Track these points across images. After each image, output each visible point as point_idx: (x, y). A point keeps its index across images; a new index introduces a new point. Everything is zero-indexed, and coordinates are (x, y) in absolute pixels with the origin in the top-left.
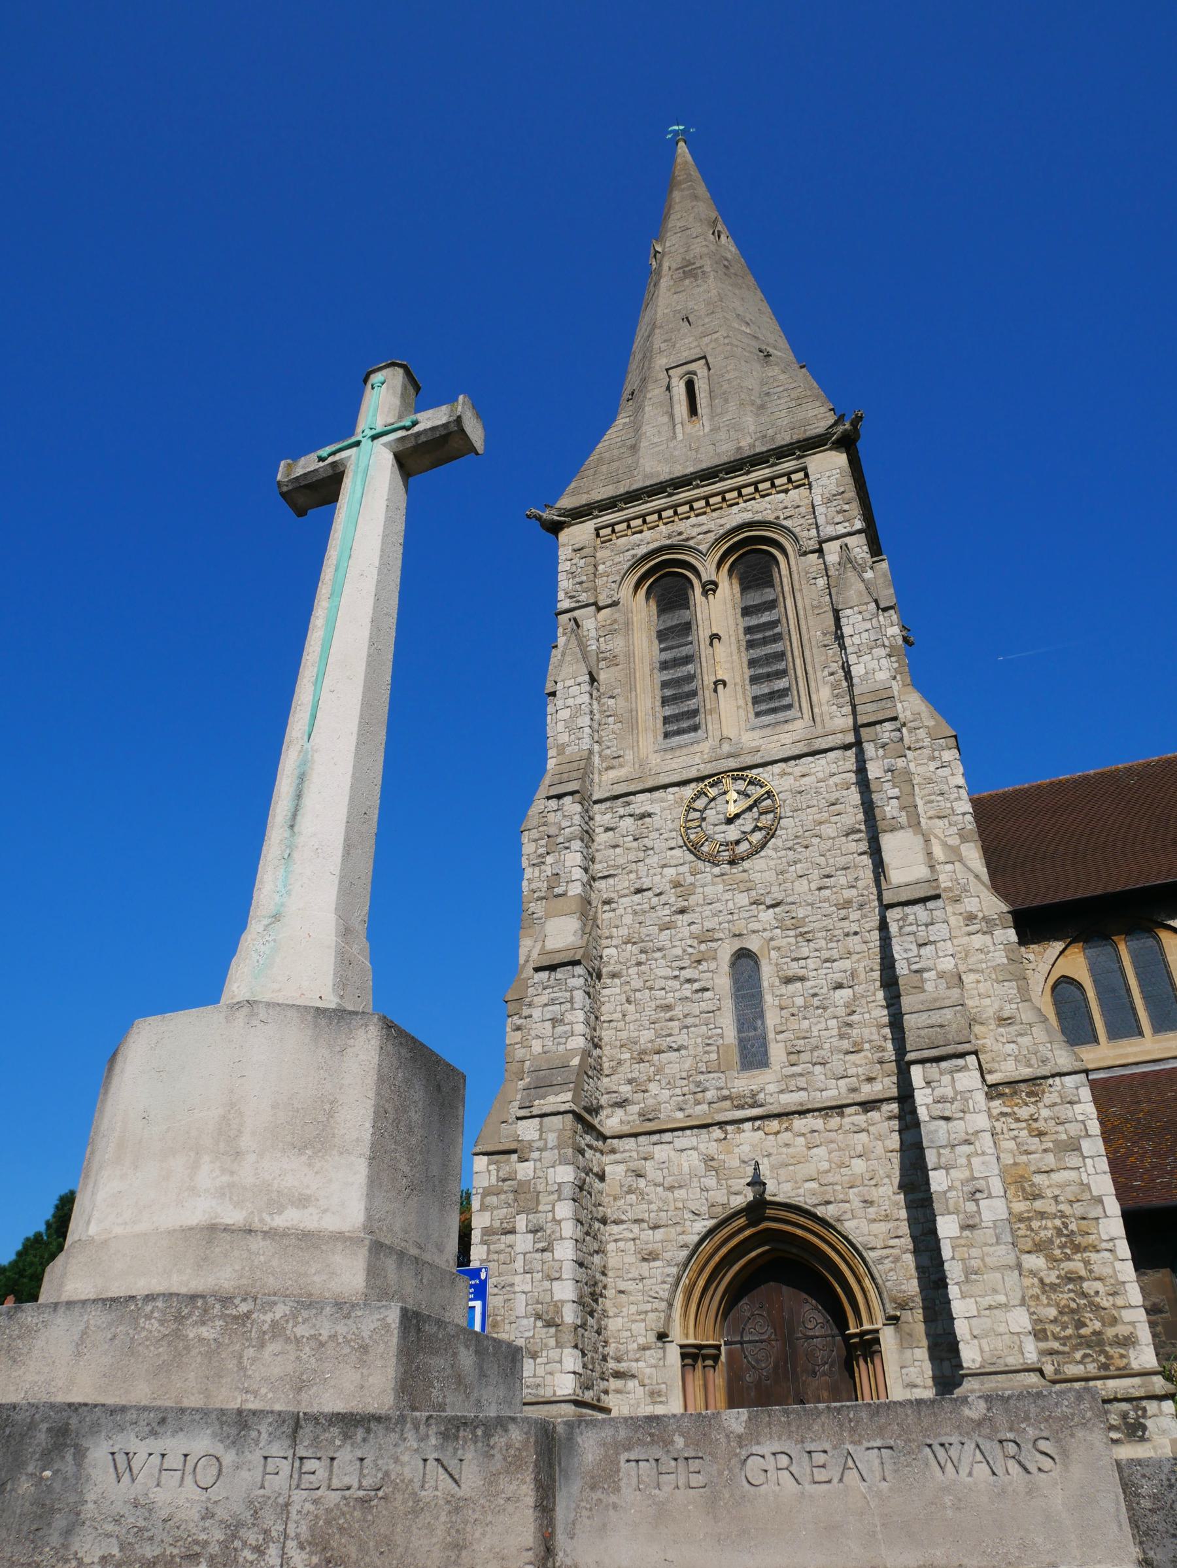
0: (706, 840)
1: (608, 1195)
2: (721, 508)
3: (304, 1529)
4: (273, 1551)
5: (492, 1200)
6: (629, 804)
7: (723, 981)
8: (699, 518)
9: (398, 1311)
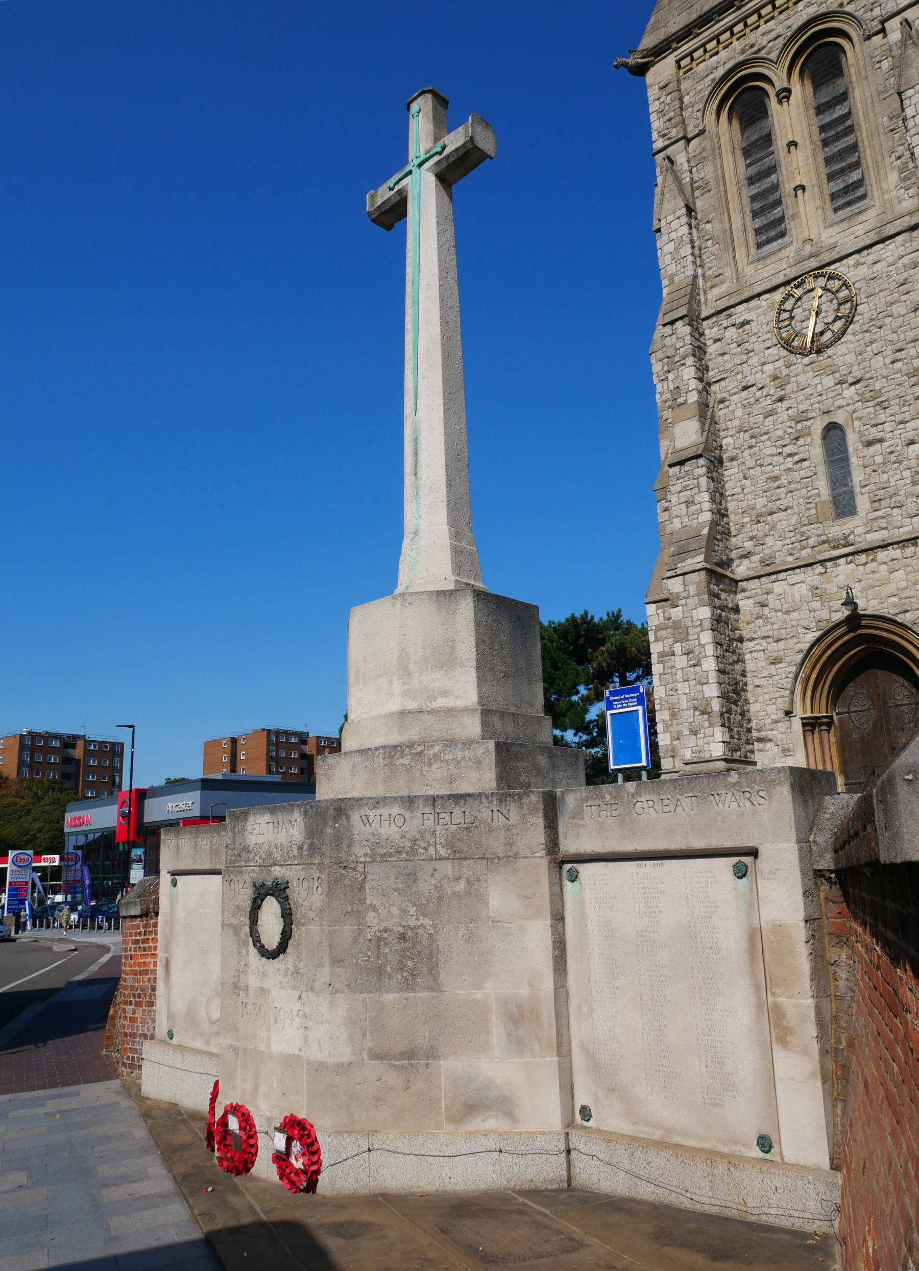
0: (796, 336)
1: (743, 622)
2: (787, 8)
3: (443, 840)
4: (431, 849)
5: (663, 633)
6: (730, 316)
7: (817, 452)
8: (769, 24)
9: (493, 744)
